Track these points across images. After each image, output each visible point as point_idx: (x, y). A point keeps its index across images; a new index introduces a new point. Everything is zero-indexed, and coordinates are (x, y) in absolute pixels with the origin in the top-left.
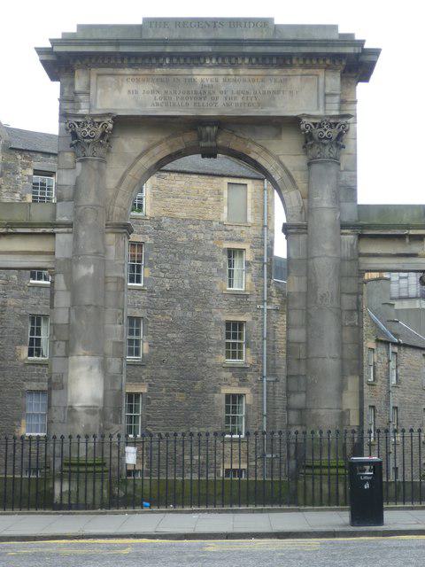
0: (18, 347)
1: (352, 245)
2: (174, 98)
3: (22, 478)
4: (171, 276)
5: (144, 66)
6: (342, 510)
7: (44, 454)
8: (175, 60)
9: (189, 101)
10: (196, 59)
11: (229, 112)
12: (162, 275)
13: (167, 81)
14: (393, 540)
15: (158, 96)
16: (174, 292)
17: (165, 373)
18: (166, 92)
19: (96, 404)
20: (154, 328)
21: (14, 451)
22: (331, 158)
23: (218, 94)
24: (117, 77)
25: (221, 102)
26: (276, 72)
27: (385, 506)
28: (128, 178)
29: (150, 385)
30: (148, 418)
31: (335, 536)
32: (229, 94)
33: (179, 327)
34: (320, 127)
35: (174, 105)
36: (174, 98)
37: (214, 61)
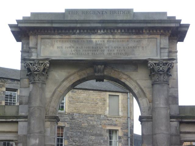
1: (176, 127)
2: (81, 50)
5: (66, 34)
8: (82, 31)
10: (93, 31)
13: (78, 41)
15: (73, 49)
18: (77, 48)
23: (104, 48)
25: (106, 52)
26: (134, 37)
28: (57, 92)
32: (110, 48)
34: (158, 65)
36: (81, 50)
37: (102, 31)
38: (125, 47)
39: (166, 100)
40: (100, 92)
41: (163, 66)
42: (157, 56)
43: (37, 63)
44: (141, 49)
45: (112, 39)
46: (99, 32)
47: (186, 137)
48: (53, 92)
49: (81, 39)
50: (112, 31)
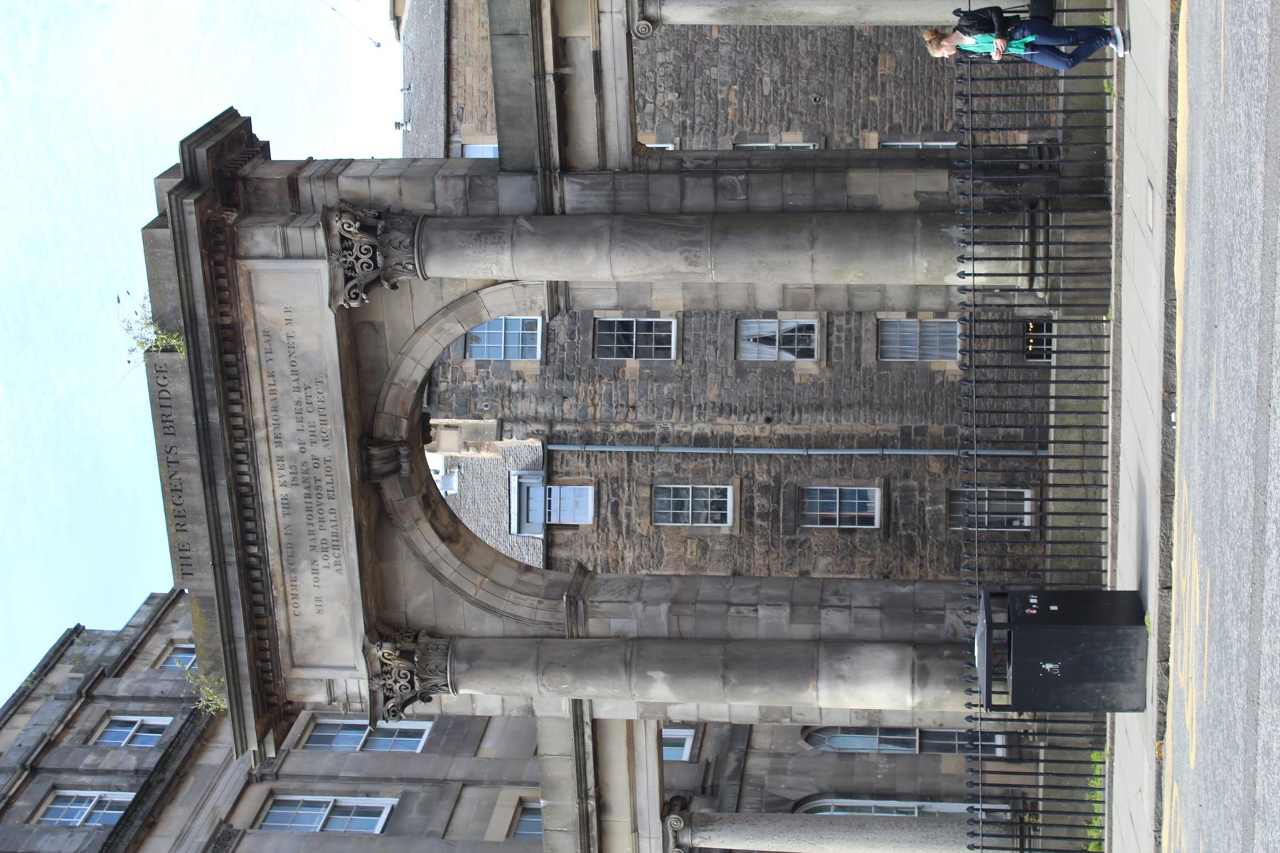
0: (797, 380)
1: (584, 187)
3: (1038, 761)
4: (650, 89)
5: (267, 589)
6: (1113, 723)
7: (996, 325)
8: (251, 537)
9: (326, 508)
11: (337, 427)
12: (649, 107)
14: (1182, 441)
15: (321, 563)
16: (683, 84)
17: (840, 98)
18: (313, 548)
19: (909, 663)
20: (753, 121)
21: (991, 381)
22: (412, 244)
23: (307, 457)
24: (294, 636)
25: (320, 451)
26: (251, 351)
27: (1109, 589)
28: (481, 596)
29: (864, 126)
30: (928, 129)
31: (1169, 623)
32: (305, 436)
33: (750, 71)
34: (352, 269)
35: (336, 535)
36: (321, 535)
37: (245, 468)
38: (295, 384)
39: (483, 239)
40: (454, 13)
41: (356, 252)
42: (318, 273)
43: (383, 682)
44: (296, 329)
45: (271, 429)
46: (247, 479)
47: (619, 145)
48: (480, 611)
49: (282, 535)
50: (239, 433)
